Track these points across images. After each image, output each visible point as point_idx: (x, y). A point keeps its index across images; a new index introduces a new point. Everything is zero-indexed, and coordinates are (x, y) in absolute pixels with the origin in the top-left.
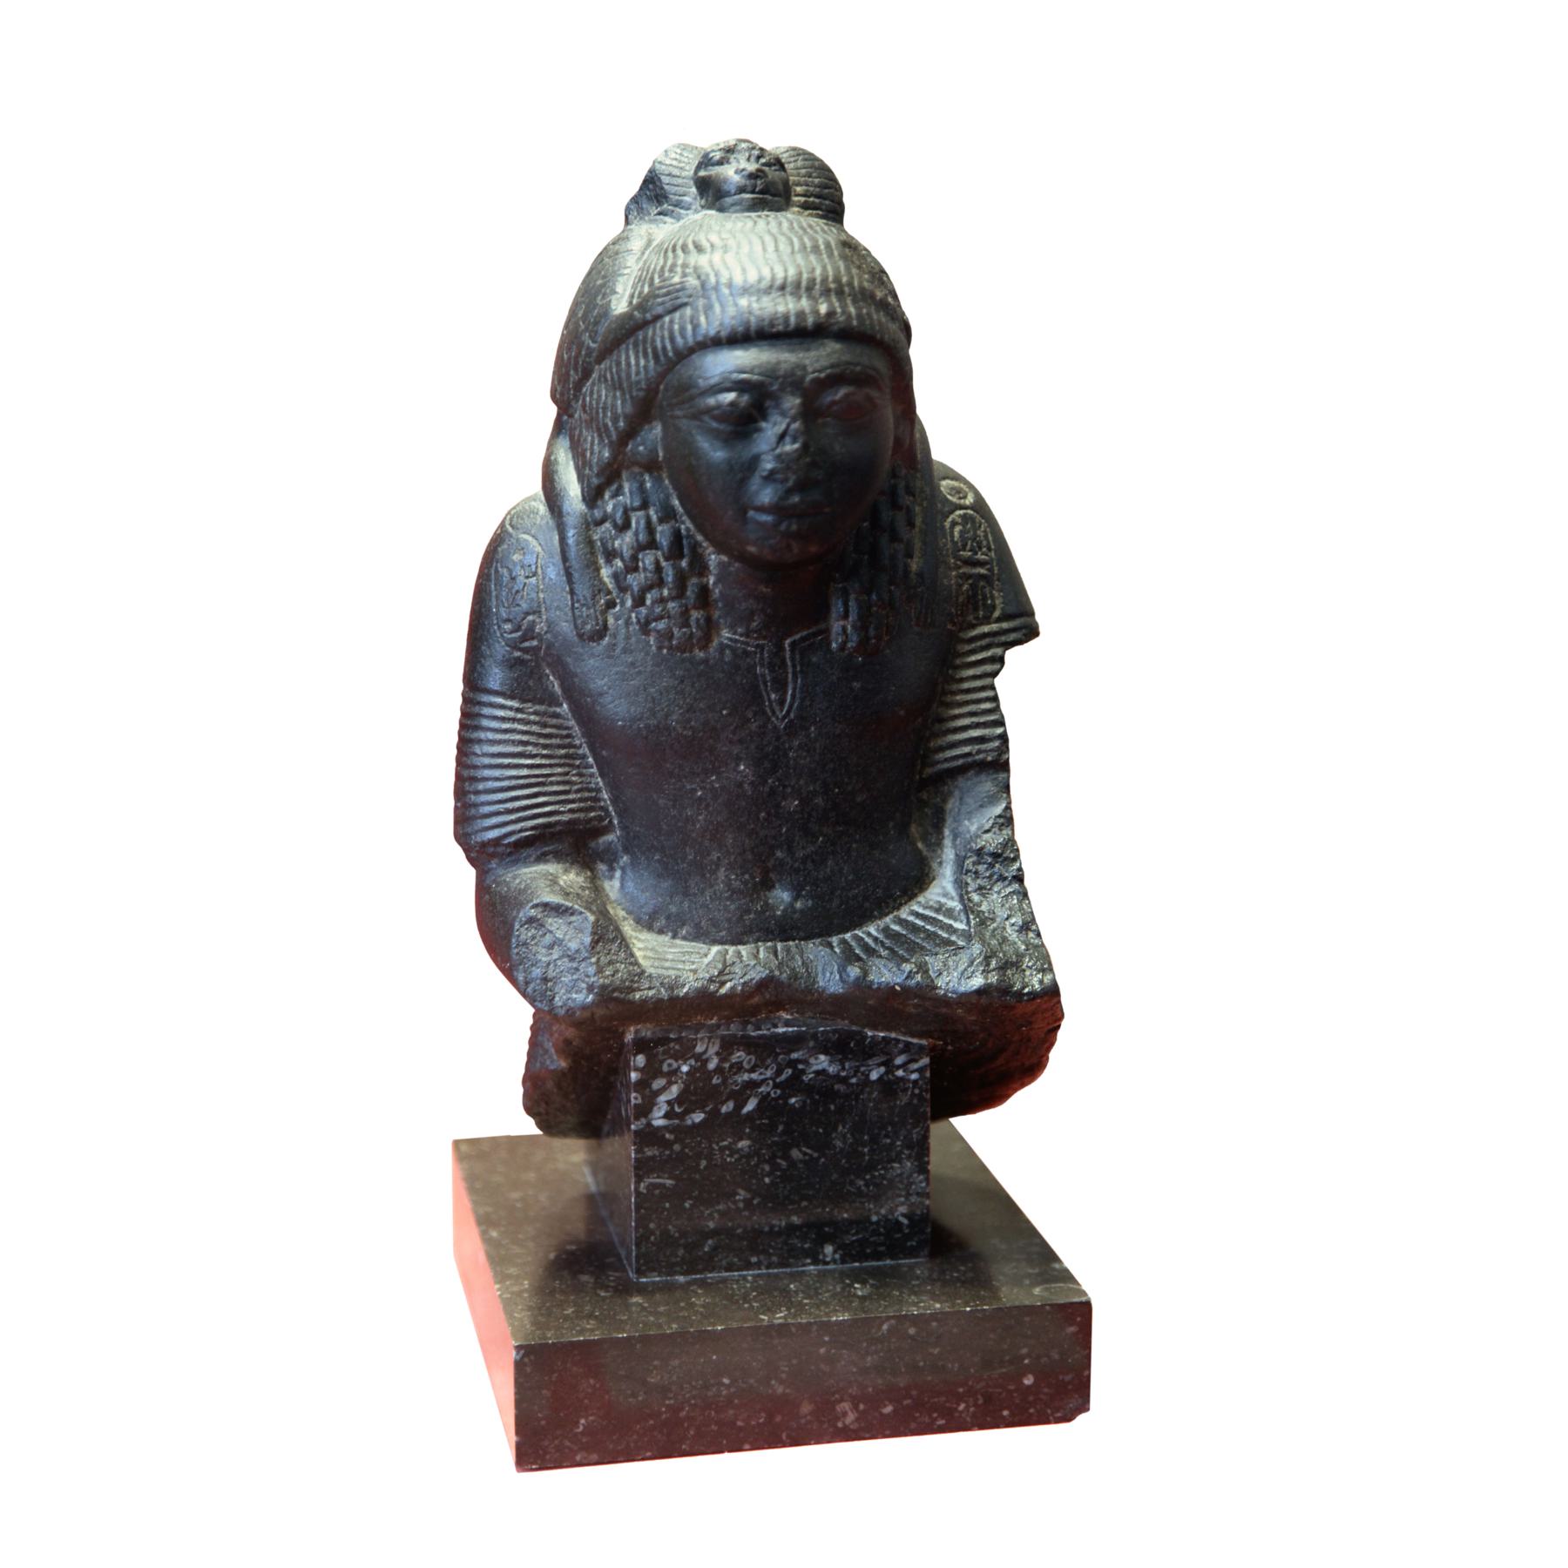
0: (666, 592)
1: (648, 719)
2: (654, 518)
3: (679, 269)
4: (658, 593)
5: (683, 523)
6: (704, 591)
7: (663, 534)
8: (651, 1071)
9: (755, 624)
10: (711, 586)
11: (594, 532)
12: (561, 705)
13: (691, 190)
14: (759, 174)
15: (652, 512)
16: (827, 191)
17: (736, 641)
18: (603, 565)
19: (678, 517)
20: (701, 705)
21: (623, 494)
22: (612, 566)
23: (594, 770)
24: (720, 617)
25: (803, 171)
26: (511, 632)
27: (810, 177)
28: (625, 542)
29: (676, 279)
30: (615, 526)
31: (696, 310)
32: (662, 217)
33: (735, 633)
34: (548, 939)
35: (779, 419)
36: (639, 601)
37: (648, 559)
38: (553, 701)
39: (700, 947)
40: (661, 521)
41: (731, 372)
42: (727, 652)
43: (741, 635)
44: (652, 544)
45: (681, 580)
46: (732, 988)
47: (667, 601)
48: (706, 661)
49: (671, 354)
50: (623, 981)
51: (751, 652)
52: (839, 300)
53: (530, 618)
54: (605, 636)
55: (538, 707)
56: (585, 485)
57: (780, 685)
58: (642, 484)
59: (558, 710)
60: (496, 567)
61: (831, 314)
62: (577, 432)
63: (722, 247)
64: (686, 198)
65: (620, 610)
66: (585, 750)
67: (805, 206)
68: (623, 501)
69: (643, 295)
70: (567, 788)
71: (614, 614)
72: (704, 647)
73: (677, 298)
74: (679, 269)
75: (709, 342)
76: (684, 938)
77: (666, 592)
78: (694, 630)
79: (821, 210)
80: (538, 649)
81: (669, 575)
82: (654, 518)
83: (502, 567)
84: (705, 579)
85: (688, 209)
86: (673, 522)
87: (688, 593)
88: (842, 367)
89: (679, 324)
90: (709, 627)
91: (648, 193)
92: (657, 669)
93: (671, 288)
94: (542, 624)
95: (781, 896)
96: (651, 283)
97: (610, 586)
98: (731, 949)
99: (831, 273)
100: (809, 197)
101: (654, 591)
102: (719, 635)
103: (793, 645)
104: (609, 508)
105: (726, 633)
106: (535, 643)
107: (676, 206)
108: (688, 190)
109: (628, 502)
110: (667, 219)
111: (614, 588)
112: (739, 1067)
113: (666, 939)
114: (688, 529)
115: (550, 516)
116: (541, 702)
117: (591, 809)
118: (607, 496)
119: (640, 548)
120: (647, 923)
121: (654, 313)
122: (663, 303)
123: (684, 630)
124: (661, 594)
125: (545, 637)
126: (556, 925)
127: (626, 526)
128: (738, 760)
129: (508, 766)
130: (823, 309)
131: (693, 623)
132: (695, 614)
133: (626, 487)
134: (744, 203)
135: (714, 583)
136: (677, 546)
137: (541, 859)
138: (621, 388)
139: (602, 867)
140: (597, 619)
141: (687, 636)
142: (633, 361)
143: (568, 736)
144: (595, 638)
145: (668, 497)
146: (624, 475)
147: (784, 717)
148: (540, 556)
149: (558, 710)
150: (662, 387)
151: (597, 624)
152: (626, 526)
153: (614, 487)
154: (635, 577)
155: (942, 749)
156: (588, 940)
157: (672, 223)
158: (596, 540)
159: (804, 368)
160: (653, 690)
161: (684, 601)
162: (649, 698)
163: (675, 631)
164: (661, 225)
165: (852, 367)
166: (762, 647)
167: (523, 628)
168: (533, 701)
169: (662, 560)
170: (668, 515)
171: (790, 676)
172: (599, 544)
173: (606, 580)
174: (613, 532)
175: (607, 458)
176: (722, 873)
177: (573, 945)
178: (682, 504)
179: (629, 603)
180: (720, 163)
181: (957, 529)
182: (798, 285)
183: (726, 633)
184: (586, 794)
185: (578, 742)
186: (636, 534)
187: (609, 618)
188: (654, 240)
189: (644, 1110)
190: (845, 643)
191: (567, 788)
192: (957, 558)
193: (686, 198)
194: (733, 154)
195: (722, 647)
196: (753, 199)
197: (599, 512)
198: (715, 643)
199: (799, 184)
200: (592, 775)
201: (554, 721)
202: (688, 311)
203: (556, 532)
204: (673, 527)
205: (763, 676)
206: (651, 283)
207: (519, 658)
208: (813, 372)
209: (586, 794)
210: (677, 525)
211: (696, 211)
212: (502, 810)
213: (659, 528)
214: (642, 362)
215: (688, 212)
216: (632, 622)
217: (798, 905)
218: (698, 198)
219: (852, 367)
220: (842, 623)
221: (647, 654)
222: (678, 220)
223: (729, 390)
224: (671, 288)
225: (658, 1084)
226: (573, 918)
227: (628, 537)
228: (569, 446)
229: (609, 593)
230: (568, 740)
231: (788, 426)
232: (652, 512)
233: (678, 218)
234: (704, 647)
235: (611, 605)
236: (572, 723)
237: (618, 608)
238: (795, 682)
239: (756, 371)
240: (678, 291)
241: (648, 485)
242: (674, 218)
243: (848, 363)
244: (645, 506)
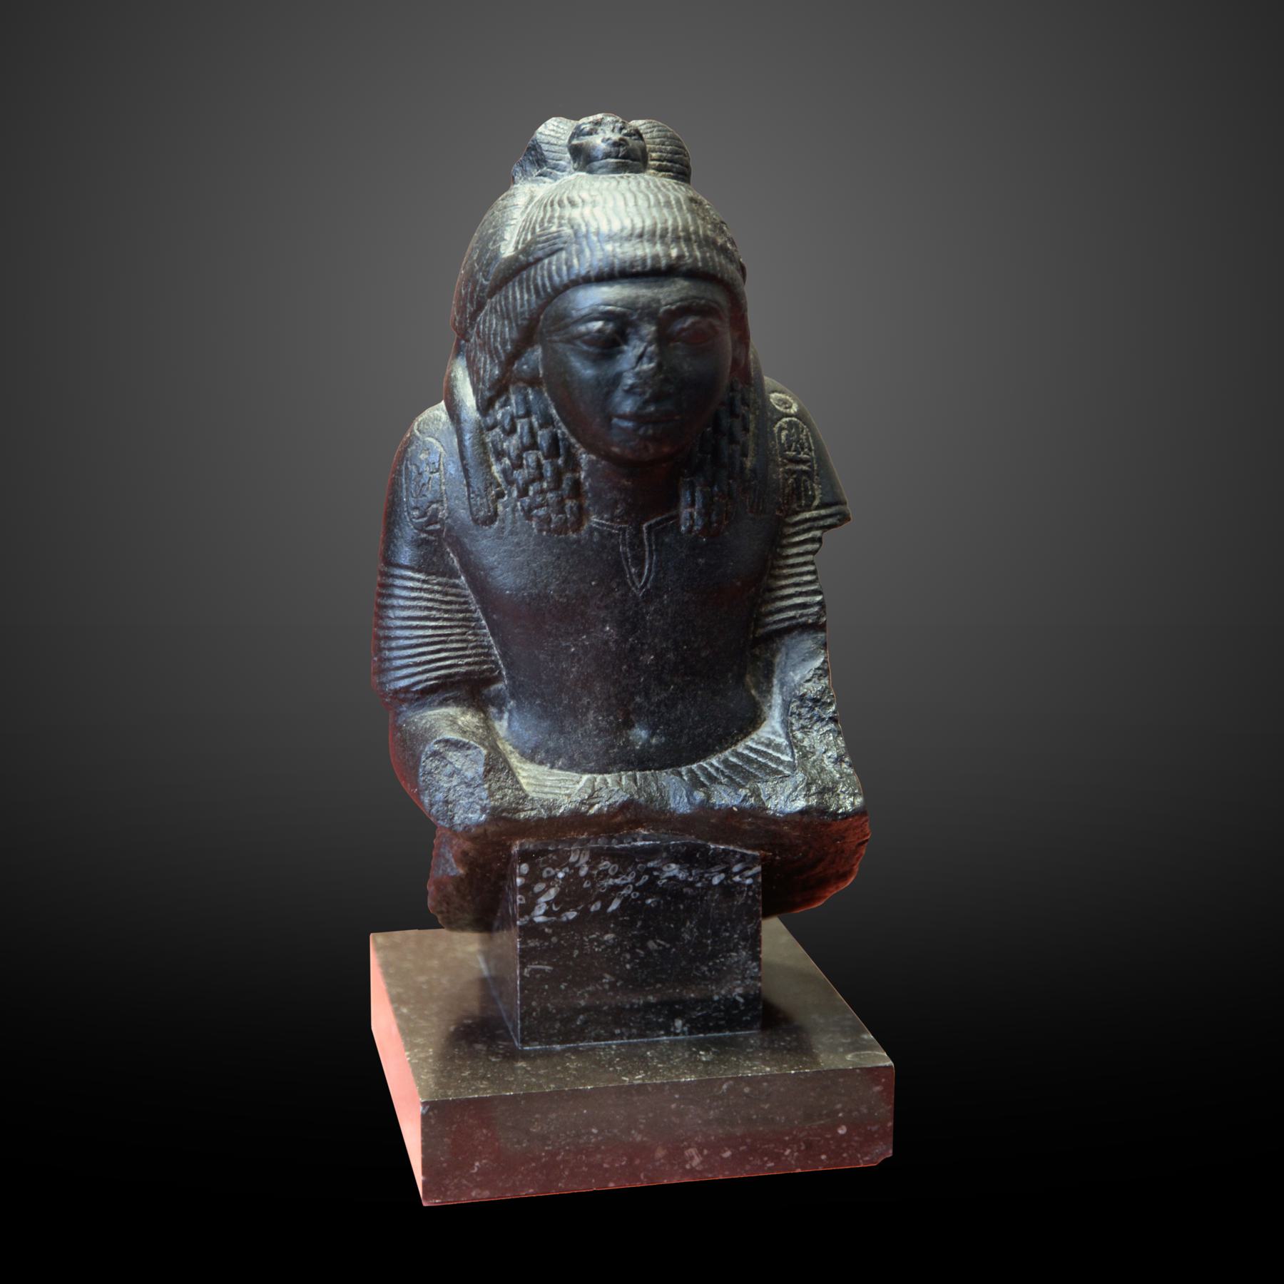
0: (545, 485)
1: (531, 589)
2: (536, 424)
3: (556, 221)
4: (539, 486)
5: (559, 428)
6: (577, 484)
7: (543, 437)
8: (533, 877)
9: (618, 511)
10: (582, 480)
11: (486, 436)
12: (459, 577)
13: (566, 156)
14: (622, 142)
15: (534, 419)
16: (677, 156)
17: (603, 525)
18: (494, 463)
19: (555, 423)
20: (574, 577)
21: (510, 405)
22: (501, 464)
23: (487, 631)
24: (589, 505)
25: (658, 140)
26: (419, 518)
27: (663, 145)
28: (512, 444)
29: (554, 229)
30: (504, 430)
31: (570, 254)
32: (542, 178)
33: (602, 519)
34: (449, 769)
35: (638, 343)
36: (523, 492)
37: (530, 458)
38: (453, 574)
40: (541, 426)
41: (599, 305)
42: (596, 534)
43: (607, 520)
44: (534, 446)
45: (558, 475)
46: (600, 809)
47: (547, 493)
48: (578, 541)
49: (549, 290)
50: (510, 803)
51: (615, 534)
52: (687, 246)
53: (434, 506)
54: (496, 521)
55: (440, 579)
56: (479, 397)
57: (639, 561)
58: (526, 396)
59: (457, 581)
60: (406, 465)
61: (680, 257)
62: (472, 354)
63: (591, 203)
64: (562, 162)
65: (508, 500)
66: (479, 614)
67: (659, 169)
68: (510, 410)
69: (526, 242)
70: (464, 645)
71: (503, 503)
72: (577, 530)
73: (554, 244)
74: (556, 221)
75: (581, 280)
76: (560, 768)
77: (545, 485)
78: (568, 516)
79: (672, 172)
80: (440, 531)
81: (548, 471)
82: (536, 424)
83: (411, 464)
84: (578, 475)
85: (564, 171)
86: (551, 427)
87: (564, 486)
88: (690, 301)
89: (556, 265)
90: (581, 513)
91: (531, 158)
92: (538, 548)
93: (550, 236)
94: (444, 511)
95: (640, 734)
96: (533, 232)
97: (500, 480)
98: (599, 777)
99: (680, 224)
100: (663, 161)
101: (535, 484)
102: (589, 520)
103: (649, 528)
104: (499, 416)
105: (594, 519)
106: (438, 526)
107: (553, 169)
108: (563, 155)
109: (515, 411)
110: (546, 179)
111: (503, 482)
112: (605, 874)
113: (545, 769)
114: (563, 434)
115: (450, 423)
116: (443, 575)
117: (484, 662)
118: (497, 406)
119: (524, 448)
120: (530, 756)
122: (543, 248)
123: (560, 516)
124: (542, 486)
125: (446, 522)
126: (455, 757)
127: (512, 431)
128: (604, 622)
129: (416, 628)
130: (674, 253)
131: (567, 510)
132: (569, 503)
133: (513, 399)
134: (609, 166)
135: (585, 478)
136: (555, 447)
137: (443, 703)
138: (508, 318)
139: (493, 710)
140: (489, 507)
141: (562, 521)
142: (518, 296)
143: (465, 603)
144: (488, 522)
145: (547, 407)
146: (511, 389)
147: (642, 587)
148: (443, 455)
149: (457, 581)
150: (542, 317)
151: (489, 511)
152: (512, 431)
153: (503, 399)
154: (520, 472)
155: (771, 613)
156: (481, 770)
157: (550, 183)
158: (488, 442)
159: (658, 301)
160: (534, 565)
161: (560, 492)
162: (531, 571)
163: (553, 516)
164: (541, 184)
165: (698, 301)
166: (624, 530)
167: (428, 514)
168: (437, 574)
169: (542, 458)
170: (547, 421)
171: (647, 553)
172: (491, 445)
173: (497, 475)
174: (502, 435)
175: (497, 375)
176: (591, 715)
177: (470, 774)
178: (558, 412)
179: (515, 494)
180: (590, 133)
181: (784, 433)
182: (653, 233)
183: (594, 519)
184: (480, 651)
186: (521, 437)
187: (498, 506)
188: (535, 196)
189: (528, 909)
190: (692, 526)
191: (464, 645)
193: (562, 162)
194: (600, 126)
195: (591, 530)
196: (617, 163)
198: (586, 527)
199: (654, 151)
200: (485, 635)
201: (454, 591)
202: (564, 255)
203: (455, 436)
204: (551, 432)
205: (625, 553)
206: (533, 232)
207: (425, 539)
208: (666, 305)
209: (480, 651)
210: (554, 430)
212: (411, 663)
213: (540, 433)
214: (526, 297)
215: (564, 173)
216: (518, 510)
217: (654, 741)
218: (572, 162)
219: (698, 301)
220: (689, 510)
221: (530, 535)
222: (556, 180)
223: (597, 319)
224: (550, 236)
225: (539, 887)
226: (469, 752)
227: (515, 440)
228: (466, 365)
229: (499, 485)
230: (465, 606)
231: (646, 349)
232: (534, 419)
233: (556, 179)
235: (500, 495)
236: (468, 592)
237: (506, 498)
238: (651, 558)
240: (555, 238)
241: (531, 397)
242: (552, 178)
243: (695, 297)
244: (528, 414)
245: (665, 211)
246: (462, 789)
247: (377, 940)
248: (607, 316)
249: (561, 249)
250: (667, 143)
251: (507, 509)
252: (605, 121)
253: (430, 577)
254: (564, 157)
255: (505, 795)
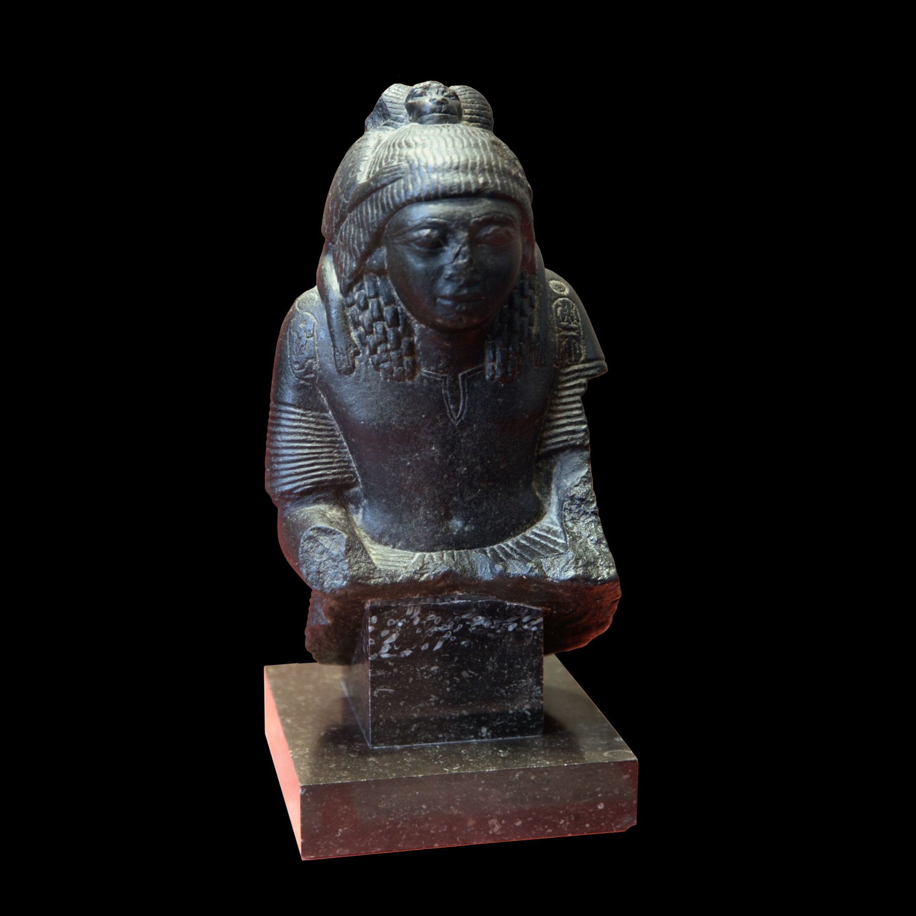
0: (389, 346)
2: (382, 303)
3: (397, 157)
4: (385, 346)
5: (399, 305)
6: (411, 345)
7: (387, 312)
8: (381, 626)
9: (441, 365)
10: (415, 343)
11: (347, 311)
12: (327, 412)
13: (404, 111)
14: (444, 101)
15: (381, 299)
16: (483, 111)
17: (430, 374)
18: (352, 330)
19: (396, 302)
20: (410, 412)
21: (364, 289)
22: (357, 331)
24: (420, 360)
26: (299, 369)
27: (473, 103)
28: (365, 317)
29: (395, 163)
30: (359, 307)
31: (406, 181)
32: (386, 127)
33: (429, 370)
34: (320, 548)
35: (455, 245)
36: (373, 351)
37: (378, 327)
38: (323, 409)
39: (409, 553)
40: (386, 304)
41: (427, 218)
42: (425, 381)
43: (433, 371)
44: (381, 318)
45: (398, 339)
46: (428, 577)
47: (390, 351)
48: (412, 386)
49: (392, 207)
50: (364, 573)
51: (439, 381)
52: (490, 175)
53: (310, 361)
54: (354, 371)
55: (314, 413)
56: (342, 284)
57: (456, 400)
58: (375, 283)
59: (326, 415)
60: (290, 331)
62: (337, 253)
63: (422, 145)
64: (401, 116)
65: (362, 356)
66: (342, 438)
67: (470, 121)
68: (364, 293)
69: (375, 173)
70: (331, 460)
71: (359, 359)
72: (411, 378)
73: (396, 174)
74: (397, 157)
75: (414, 200)
76: (400, 548)
77: (389, 346)
78: (406, 368)
79: (480, 122)
80: (314, 379)
81: (391, 336)
82: (382, 303)
83: (293, 331)
84: (412, 339)
85: (402, 122)
86: (393, 305)
87: (402, 346)
88: (492, 215)
89: (397, 189)
90: (414, 366)
91: (379, 113)
92: (384, 391)
93: (392, 168)
94: (317, 365)
95: (457, 524)
96: (381, 165)
97: (357, 342)
98: (427, 555)
99: (485, 160)
100: (473, 115)
101: (382, 345)
102: (420, 371)
103: (463, 377)
105: (424, 370)
106: (312, 376)
107: (395, 120)
108: (402, 111)
109: (367, 293)
110: (390, 128)
111: (359, 344)
112: (431, 624)
113: (389, 548)
114: (402, 309)
115: (321, 301)
116: (316, 410)
117: (345, 473)
118: (355, 290)
119: (374, 320)
120: (378, 539)
121: (382, 183)
122: (387, 177)
123: (400, 368)
124: (386, 347)
125: (318, 372)
126: (325, 540)
128: (431, 444)
129: (297, 448)
130: (481, 180)
131: (405, 364)
132: (406, 359)
133: (366, 284)
134: (434, 119)
135: (417, 341)
136: (396, 319)
137: (316, 502)
138: (363, 227)
139: (352, 507)
140: (349, 362)
142: (370, 211)
143: (332, 430)
144: (348, 373)
145: (390, 290)
146: (365, 278)
147: (458, 419)
148: (316, 325)
149: (326, 415)
150: (387, 226)
151: (349, 365)
152: (365, 307)
153: (359, 284)
154: (371, 337)
155: (550, 438)
156: (343, 549)
157: (393, 131)
158: (348, 315)
159: (470, 215)
160: (381, 403)
161: (399, 351)
162: (379, 408)
163: (395, 368)
164: (386, 132)
165: (498, 215)
166: (445, 378)
167: (306, 367)
168: (312, 409)
169: (387, 327)
170: (390, 301)
171: (462, 395)
172: (350, 318)
173: (354, 339)
174: (358, 311)
175: (355, 268)
176: (422, 510)
177: (335, 552)
178: (398, 294)
179: (367, 352)
180: (421, 95)
181: (559, 309)
182: (466, 166)
183: (424, 370)
184: (343, 464)
185: (337, 434)
186: (372, 312)
187: (355, 361)
188: (382, 140)
189: (376, 648)
190: (493, 375)
191: (331, 460)
192: (559, 326)
193: (401, 116)
194: (428, 90)
195: (422, 378)
196: (440, 116)
197: (350, 299)
198: (418, 376)
199: (466, 108)
200: (346, 453)
201: (324, 421)
202: (402, 182)
203: (325, 311)
204: (393, 308)
205: (446, 395)
206: (381, 165)
207: (303, 384)
208: (475, 218)
209: (343, 464)
210: (396, 307)
211: (407, 123)
212: (293, 473)
213: (385, 309)
214: (375, 212)
215: (402, 124)
216: (369, 363)
217: (466, 529)
218: (408, 116)
219: (498, 215)
220: (492, 364)
221: (378, 382)
222: (396, 129)
223: (426, 228)
224: (392, 168)
225: (384, 633)
226: (335, 536)
227: (367, 314)
228: (332, 260)
229: (356, 346)
230: (332, 432)
231: (460, 249)
232: (381, 299)
233: (396, 127)
234: (411, 378)
235: (357, 353)
236: (334, 422)
237: (361, 355)
238: (464, 398)
239: (442, 217)
240: (396, 170)
241: (379, 283)
242: (394, 127)
243: (496, 212)
244: (377, 295)
245: (475, 151)
246: (330, 563)
247: (269, 671)
248: (433, 226)
249: (400, 178)
250: (476, 102)
251: (362, 363)
252: (432, 86)
253: (307, 412)
254: (403, 112)
255: (360, 567)
